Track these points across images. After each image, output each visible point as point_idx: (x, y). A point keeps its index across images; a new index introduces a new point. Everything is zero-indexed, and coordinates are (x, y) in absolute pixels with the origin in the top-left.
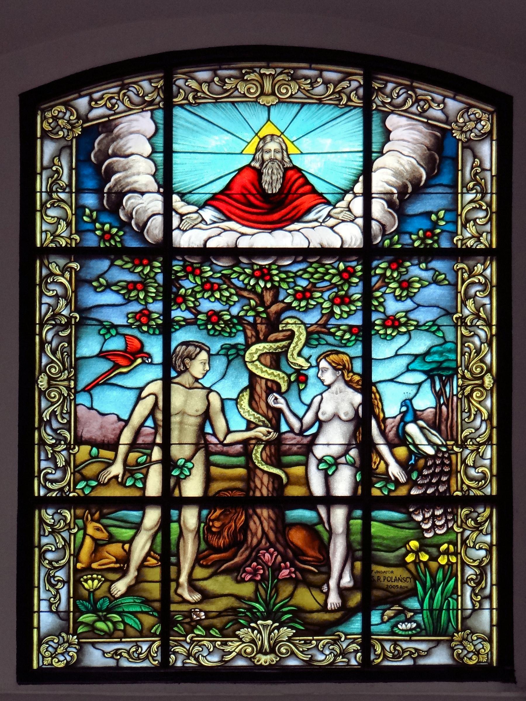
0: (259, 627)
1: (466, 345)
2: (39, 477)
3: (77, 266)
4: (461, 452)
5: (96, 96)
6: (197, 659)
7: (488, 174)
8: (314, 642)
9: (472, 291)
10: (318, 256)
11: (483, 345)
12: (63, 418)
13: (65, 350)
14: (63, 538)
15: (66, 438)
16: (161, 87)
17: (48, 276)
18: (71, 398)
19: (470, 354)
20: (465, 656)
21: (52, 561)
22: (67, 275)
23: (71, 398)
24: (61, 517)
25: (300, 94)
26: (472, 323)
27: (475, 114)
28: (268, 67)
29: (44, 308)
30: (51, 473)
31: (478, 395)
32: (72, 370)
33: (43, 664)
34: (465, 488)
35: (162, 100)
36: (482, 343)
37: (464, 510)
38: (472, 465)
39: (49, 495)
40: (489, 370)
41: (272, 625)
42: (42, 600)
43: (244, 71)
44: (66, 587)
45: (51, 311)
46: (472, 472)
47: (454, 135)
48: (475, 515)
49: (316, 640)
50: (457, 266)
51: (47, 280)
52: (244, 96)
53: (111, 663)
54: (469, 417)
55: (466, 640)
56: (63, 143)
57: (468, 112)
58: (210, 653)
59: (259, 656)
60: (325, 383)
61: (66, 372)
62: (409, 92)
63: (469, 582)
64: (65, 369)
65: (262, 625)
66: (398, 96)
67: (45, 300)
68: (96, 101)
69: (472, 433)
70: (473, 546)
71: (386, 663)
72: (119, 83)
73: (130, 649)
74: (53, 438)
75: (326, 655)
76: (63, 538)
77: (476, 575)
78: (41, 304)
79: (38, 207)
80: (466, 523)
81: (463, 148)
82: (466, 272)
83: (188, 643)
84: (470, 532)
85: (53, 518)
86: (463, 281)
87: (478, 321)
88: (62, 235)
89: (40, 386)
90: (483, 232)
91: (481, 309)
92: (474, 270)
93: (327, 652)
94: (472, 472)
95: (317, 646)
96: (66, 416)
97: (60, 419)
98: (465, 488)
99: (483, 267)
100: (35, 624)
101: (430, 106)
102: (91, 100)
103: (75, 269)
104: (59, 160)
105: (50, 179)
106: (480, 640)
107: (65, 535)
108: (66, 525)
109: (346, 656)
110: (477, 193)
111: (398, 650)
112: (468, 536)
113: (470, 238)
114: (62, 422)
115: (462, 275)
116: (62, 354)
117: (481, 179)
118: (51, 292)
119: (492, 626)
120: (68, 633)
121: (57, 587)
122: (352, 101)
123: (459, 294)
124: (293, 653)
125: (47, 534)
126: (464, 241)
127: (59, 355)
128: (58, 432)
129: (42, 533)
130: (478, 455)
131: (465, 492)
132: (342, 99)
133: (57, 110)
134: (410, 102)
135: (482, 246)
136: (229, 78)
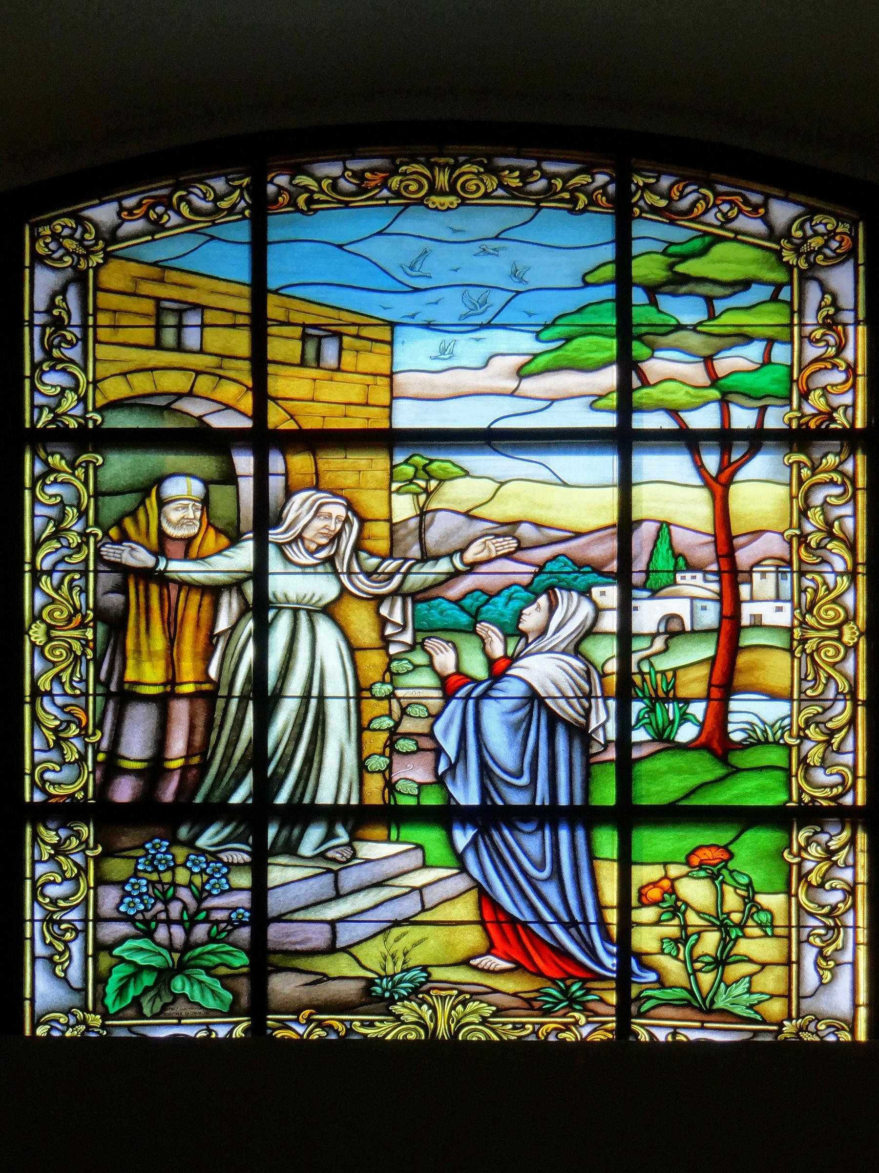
2: (32, 775)
4: (799, 746)
5: (129, 203)
7: (40, 950)
12: (73, 688)
14: (76, 864)
16: (247, 185)
17: (44, 476)
21: (832, 369)
24: (71, 832)
25: (500, 192)
27: (826, 224)
30: (54, 771)
31: (59, 613)
32: (89, 612)
34: (806, 799)
35: (249, 206)
37: (801, 833)
39: (53, 801)
42: (39, 958)
46: (66, 493)
48: (824, 837)
49: (533, 1024)
50: (789, 459)
51: (844, 789)
54: (73, 580)
64: (811, 655)
66: (682, 197)
67: (848, 759)
72: (171, 182)
74: (830, 550)
76: (76, 864)
79: (27, 372)
85: (57, 835)
87: (829, 542)
88: (72, 413)
89: (33, 639)
90: (839, 407)
92: (821, 463)
94: (66, 493)
96: (81, 686)
100: (28, 994)
102: (121, 209)
103: (94, 463)
104: (64, 300)
106: (832, 1029)
107: (78, 858)
108: (81, 843)
113: (814, 416)
115: (799, 473)
116: (71, 589)
118: (835, 771)
119: (855, 1006)
120: (85, 1009)
125: (841, 410)
126: (83, 847)
129: (850, 411)
133: (59, 224)
134: (701, 206)
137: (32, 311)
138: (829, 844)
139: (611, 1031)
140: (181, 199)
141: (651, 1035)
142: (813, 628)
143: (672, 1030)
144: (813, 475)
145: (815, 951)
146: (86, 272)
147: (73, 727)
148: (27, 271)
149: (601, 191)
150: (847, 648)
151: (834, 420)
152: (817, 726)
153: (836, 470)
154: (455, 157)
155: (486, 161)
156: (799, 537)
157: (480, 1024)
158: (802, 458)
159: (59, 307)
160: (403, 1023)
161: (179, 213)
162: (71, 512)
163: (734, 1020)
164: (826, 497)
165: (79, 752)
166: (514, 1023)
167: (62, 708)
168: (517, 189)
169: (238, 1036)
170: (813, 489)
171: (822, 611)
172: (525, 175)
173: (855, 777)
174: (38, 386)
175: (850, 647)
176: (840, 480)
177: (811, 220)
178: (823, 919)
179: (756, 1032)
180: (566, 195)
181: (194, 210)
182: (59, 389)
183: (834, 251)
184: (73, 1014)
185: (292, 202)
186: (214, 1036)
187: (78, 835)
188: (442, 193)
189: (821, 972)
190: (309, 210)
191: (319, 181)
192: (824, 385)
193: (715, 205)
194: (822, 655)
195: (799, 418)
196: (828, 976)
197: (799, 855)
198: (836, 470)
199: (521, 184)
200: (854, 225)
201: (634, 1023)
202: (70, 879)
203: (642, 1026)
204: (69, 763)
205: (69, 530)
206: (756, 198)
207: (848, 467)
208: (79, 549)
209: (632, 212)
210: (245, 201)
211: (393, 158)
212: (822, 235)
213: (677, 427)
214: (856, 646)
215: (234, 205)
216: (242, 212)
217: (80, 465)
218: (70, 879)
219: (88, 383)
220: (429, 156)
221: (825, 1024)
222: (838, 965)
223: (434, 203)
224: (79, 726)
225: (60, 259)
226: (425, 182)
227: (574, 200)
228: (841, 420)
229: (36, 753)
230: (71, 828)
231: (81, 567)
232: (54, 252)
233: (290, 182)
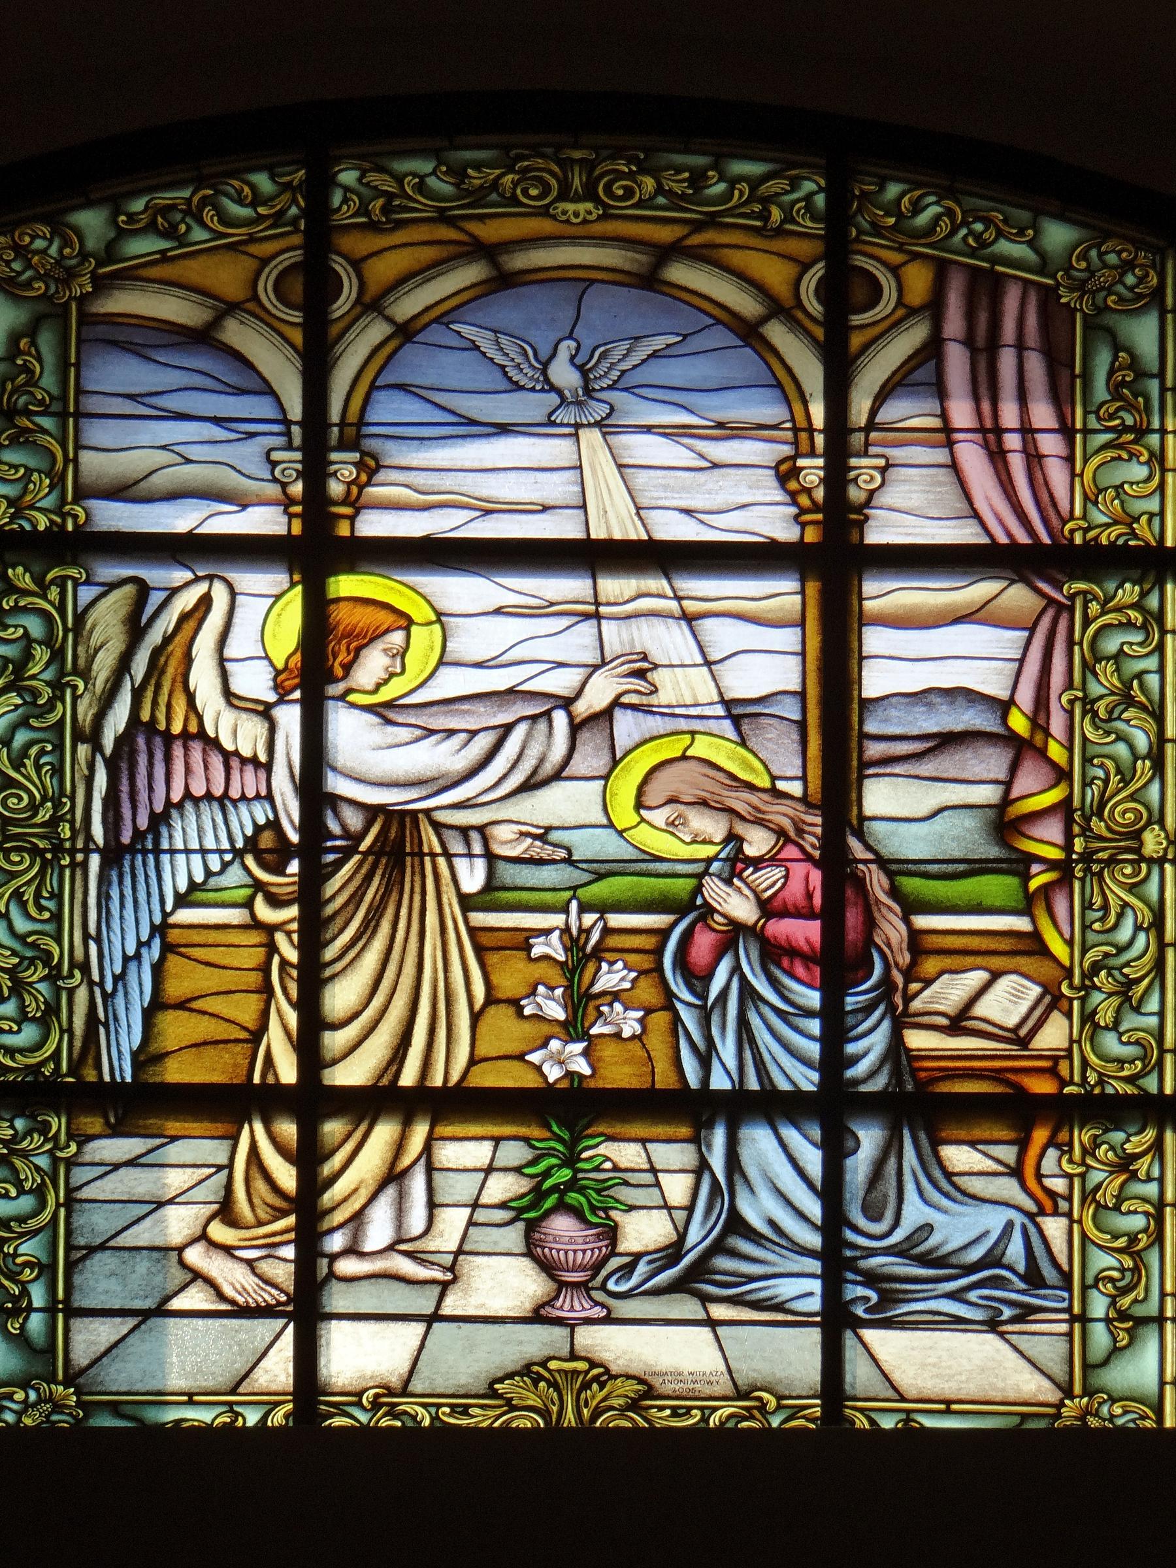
0: (553, 1376)
1: (47, 915)
3: (80, 573)
11: (1139, 762)
12: (41, 909)
14: (38, 1169)
15: (49, 954)
16: (301, 182)
18: (63, 862)
19: (1106, 782)
25: (661, 200)
26: (1111, 712)
28: (577, 146)
30: (1131, 644)
31: (15, 801)
32: (64, 800)
36: (1136, 757)
38: (35, 645)
41: (587, 1372)
47: (1063, 300)
48: (1119, 1136)
49: (702, 1408)
51: (1144, 1067)
56: (42, 307)
60: (717, 840)
65: (559, 1371)
69: (37, 717)
77: (1122, 1270)
80: (1094, 1156)
81: (1086, 327)
84: (1103, 1175)
85: (12, 1127)
86: (1087, 622)
87: (1125, 710)
91: (1135, 683)
96: (51, 905)
97: (1109, 764)
98: (1092, 1078)
112: (1100, 1184)
114: (38, 917)
116: (1105, 907)
117: (1136, 396)
118: (12, 630)
122: (794, 221)
123: (1076, 648)
125: (1144, 519)
128: (1113, 736)
129: (1156, 521)
130: (1127, 1004)
131: (1093, 1087)
132: (770, 213)
136: (478, 166)
139: (813, 1420)
140: (204, 201)
141: (872, 1422)
145: (1106, 1301)
149: (803, 204)
150: (1150, 861)
151: (1136, 536)
152: (1109, 974)
153: (1136, 606)
154: (595, 149)
155: (642, 156)
156: (59, 976)
162: (41, 654)
164: (1123, 644)
165: (1095, 675)
166: (674, 1408)
169: (276, 1424)
170: (1107, 632)
171: (1118, 809)
172: (698, 179)
176: (1140, 619)
177: (1099, 246)
178: (30, 425)
179: (1025, 1417)
180: (757, 208)
182: (22, 471)
183: (1131, 289)
184: (33, 1388)
185: (362, 211)
186: (240, 1422)
187: (44, 1128)
188: (577, 199)
189: (33, 350)
191: (399, 179)
192: (1118, 483)
193: (965, 223)
195: (1086, 530)
198: (1136, 606)
201: (848, 1407)
202: (30, 1191)
203: (862, 1410)
204: (1108, 659)
205: (1110, 995)
206: (1024, 216)
208: (1096, 968)
210: (298, 206)
211: (507, 148)
212: (1115, 267)
215: (282, 212)
216: (294, 221)
217: (52, 582)
218: (30, 1191)
220: (559, 148)
221: (1122, 1407)
223: (564, 212)
225: (28, 285)
226: (553, 182)
227: (765, 216)
230: (32, 1117)
232: (19, 274)
233: (360, 180)
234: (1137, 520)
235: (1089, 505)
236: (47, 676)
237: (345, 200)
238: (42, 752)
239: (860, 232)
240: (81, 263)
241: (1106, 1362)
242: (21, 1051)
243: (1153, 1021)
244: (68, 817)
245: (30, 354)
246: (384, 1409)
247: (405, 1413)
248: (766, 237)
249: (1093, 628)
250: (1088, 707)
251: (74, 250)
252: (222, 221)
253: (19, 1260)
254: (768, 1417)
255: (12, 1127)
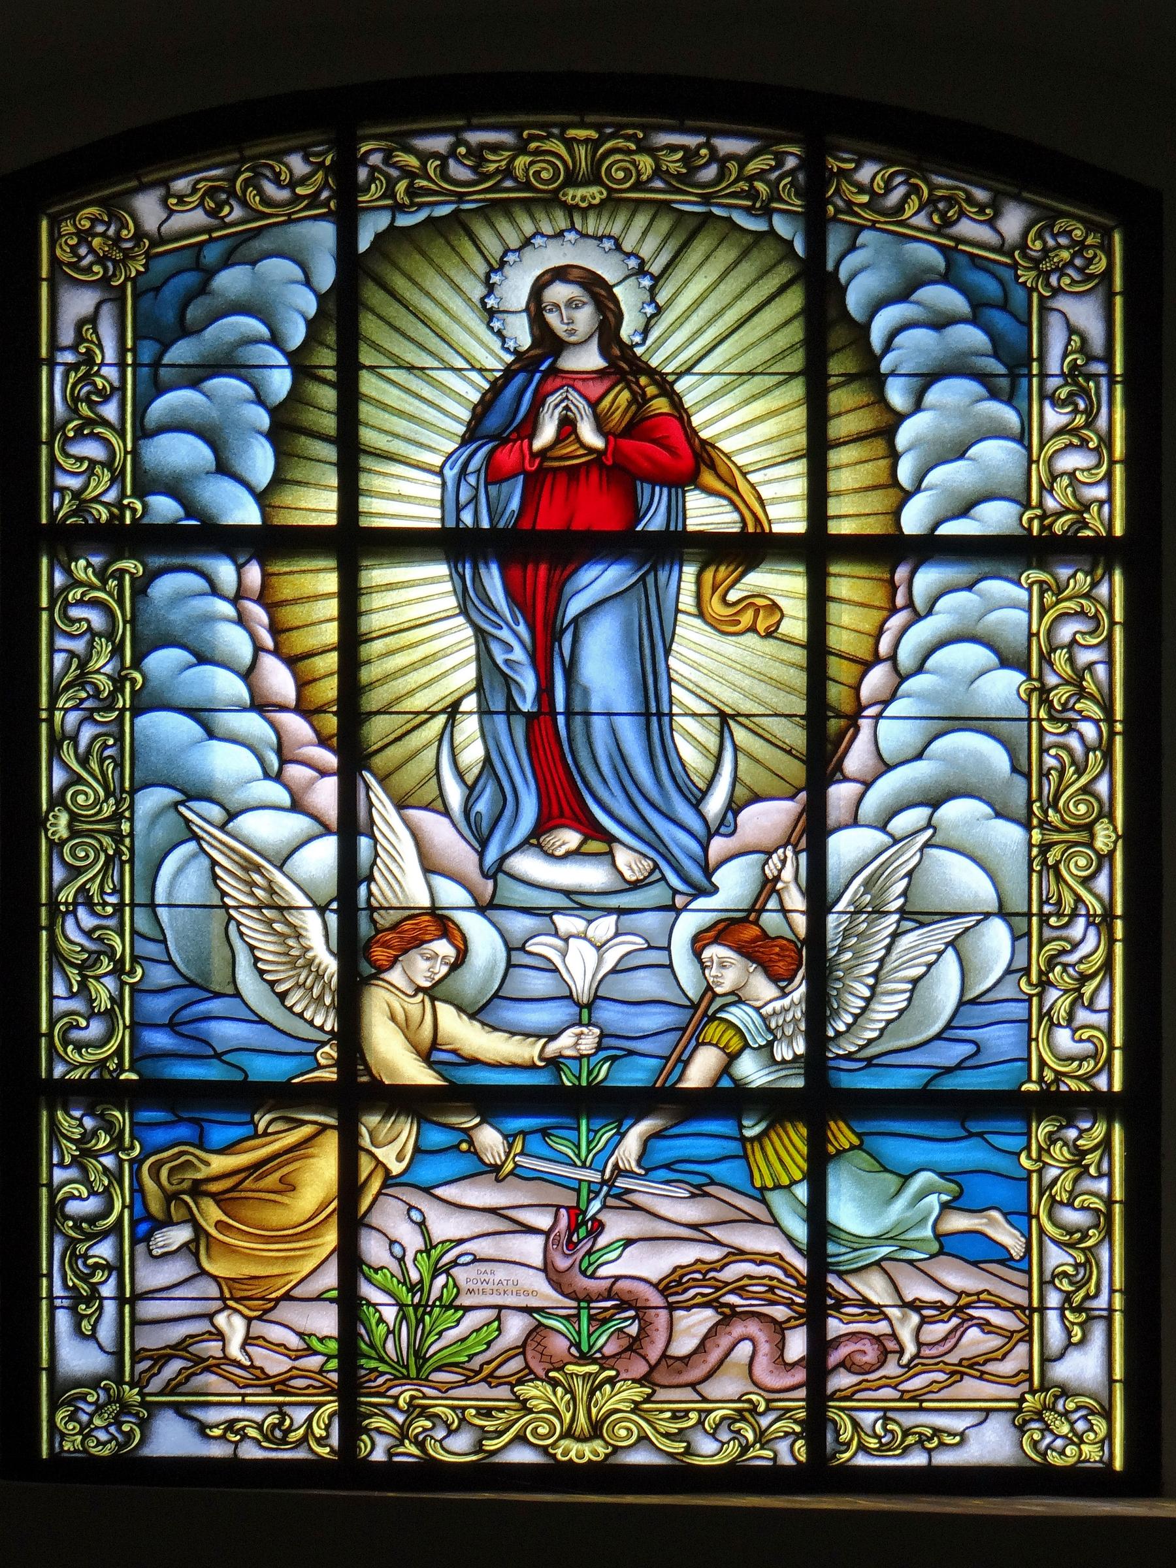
5: (181, 185)
6: (421, 1445)
8: (694, 1416)
9: (96, 1029)
10: (809, 1270)
13: (107, 753)
17: (66, 589)
18: (124, 858)
20: (1049, 1447)
22: (112, 583)
23: (124, 858)
25: (658, 184)
29: (59, 660)
33: (62, 1451)
34: (1049, 1076)
36: (1088, 749)
40: (56, 846)
41: (597, 1374)
43: (525, 133)
44: (112, 1282)
45: (74, 667)
48: (1072, 1134)
49: (700, 1411)
52: (528, 186)
53: (218, 1451)
55: (1053, 1409)
57: (1052, 227)
58: (450, 1432)
59: (565, 1443)
61: (112, 801)
62: (913, 181)
63: (1057, 1282)
68: (181, 199)
70: (1068, 1199)
71: (862, 1460)
73: (264, 1421)
75: (723, 1444)
78: (52, 651)
82: (1050, 588)
83: (401, 1411)
86: (119, 1052)
87: (1078, 701)
93: (724, 1436)
95: (701, 1422)
98: (1049, 1076)
99: (1089, 579)
101: (962, 214)
103: (132, 574)
104: (96, 332)
105: (73, 374)
106: (1083, 1412)
107: (108, 1161)
109: (770, 1445)
110: (1076, 411)
111: (892, 1432)
115: (1041, 597)
116: (101, 761)
119: (1111, 1381)
121: (94, 1280)
124: (643, 1438)
125: (68, 1160)
126: (1047, 522)
127: (94, 765)
129: (1106, 508)
131: (1049, 1085)
135: (1090, 533)
137: (54, 347)
138: (1079, 1142)
139: (796, 1421)
142: (1058, 830)
143: (880, 1414)
144: (1058, 602)
146: (123, 287)
147: (106, 961)
148: (44, 288)
149: (790, 179)
150: (1100, 857)
151: (1086, 525)
152: (1065, 970)
154: (598, 127)
155: (641, 135)
157: (633, 1411)
158: (1043, 576)
159: (87, 341)
160: (530, 1411)
161: (244, 203)
163: (986, 263)
165: (1051, 664)
166: (674, 1411)
167: (88, 934)
168: (679, 177)
170: (1053, 460)
173: (1112, 1048)
174: (60, 459)
175: (1104, 856)
176: (1093, 610)
181: (266, 201)
182: (86, 465)
185: (389, 193)
190: (412, 204)
194: (1072, 866)
196: (1077, 1332)
197: (1039, 1159)
199: (684, 171)
200: (1107, 234)
204: (1062, 648)
205: (1066, 991)
207: (1103, 590)
209: (825, 211)
213: (829, 1338)
214: (1111, 854)
215: (317, 194)
216: (326, 204)
217: (112, 576)
219: (126, 453)
220: (564, 127)
222: (1090, 1319)
224: (111, 958)
228: (1095, 524)
229: (55, 1001)
231: (114, 729)
234: (1087, 507)
235: (1045, 494)
236: (108, 669)
237: (372, 179)
238: (105, 747)
239: (838, 211)
240: (137, 245)
241: (1061, 1356)
242: (88, 1045)
243: (1101, 1019)
244: (127, 814)
245: (92, 342)
246: (418, 1410)
247: (437, 1416)
248: (756, 216)
249: (1048, 619)
250: (1044, 696)
251: (129, 231)
252: (263, 202)
253: (91, 1261)
254: (758, 1418)
255: (81, 1125)
